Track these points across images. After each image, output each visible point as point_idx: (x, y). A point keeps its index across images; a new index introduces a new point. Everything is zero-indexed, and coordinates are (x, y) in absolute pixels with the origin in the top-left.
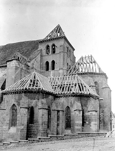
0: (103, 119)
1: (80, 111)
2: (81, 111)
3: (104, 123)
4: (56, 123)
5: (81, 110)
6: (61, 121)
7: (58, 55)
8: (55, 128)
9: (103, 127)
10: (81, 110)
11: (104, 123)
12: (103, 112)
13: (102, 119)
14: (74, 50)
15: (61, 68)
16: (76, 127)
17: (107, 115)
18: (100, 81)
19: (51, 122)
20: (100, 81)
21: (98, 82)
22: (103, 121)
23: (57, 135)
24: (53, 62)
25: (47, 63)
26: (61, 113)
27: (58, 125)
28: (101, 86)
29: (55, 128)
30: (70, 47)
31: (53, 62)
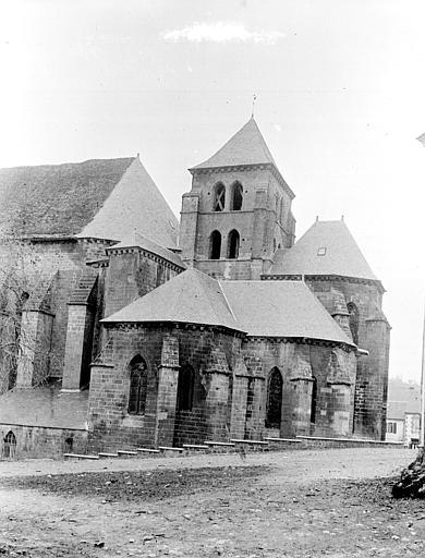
9: (361, 426)
14: (292, 196)
18: (362, 302)
20: (362, 302)
21: (357, 305)
22: (363, 410)
24: (234, 235)
25: (216, 236)
31: (234, 235)
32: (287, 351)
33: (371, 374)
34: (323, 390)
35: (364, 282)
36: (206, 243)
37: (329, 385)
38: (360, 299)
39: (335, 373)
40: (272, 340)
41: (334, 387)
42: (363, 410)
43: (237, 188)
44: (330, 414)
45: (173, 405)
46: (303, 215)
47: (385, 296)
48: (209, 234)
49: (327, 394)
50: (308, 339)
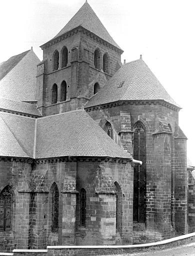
0: (154, 206)
1: (70, 196)
2: (72, 195)
3: (156, 215)
4: (26, 220)
5: (73, 193)
6: (38, 215)
7: (70, 68)
8: (26, 230)
9: (153, 222)
10: (73, 193)
11: (156, 215)
12: (154, 190)
13: (151, 206)
14: (120, 52)
15: (73, 96)
16: (64, 231)
17: (161, 198)
18: (148, 120)
19: (14, 217)
20: (148, 120)
21: (144, 122)
22: (153, 210)
23: (29, 248)
24: (64, 84)
25: (55, 86)
26: (38, 198)
27: (32, 223)
28: (150, 131)
29: (25, 229)
30: (104, 47)
31: (64, 84)
32: (61, 169)
33: (158, 179)
34: (92, 199)
35: (149, 102)
36: (50, 93)
37: (97, 195)
38: (146, 117)
39: (101, 184)
40: (52, 160)
41: (100, 196)
42: (153, 210)
43: (65, 50)
44: (98, 219)
45: (75, 204)
46: (127, 57)
47: (180, 113)
48: (52, 85)
49: (96, 203)
50: (72, 158)
